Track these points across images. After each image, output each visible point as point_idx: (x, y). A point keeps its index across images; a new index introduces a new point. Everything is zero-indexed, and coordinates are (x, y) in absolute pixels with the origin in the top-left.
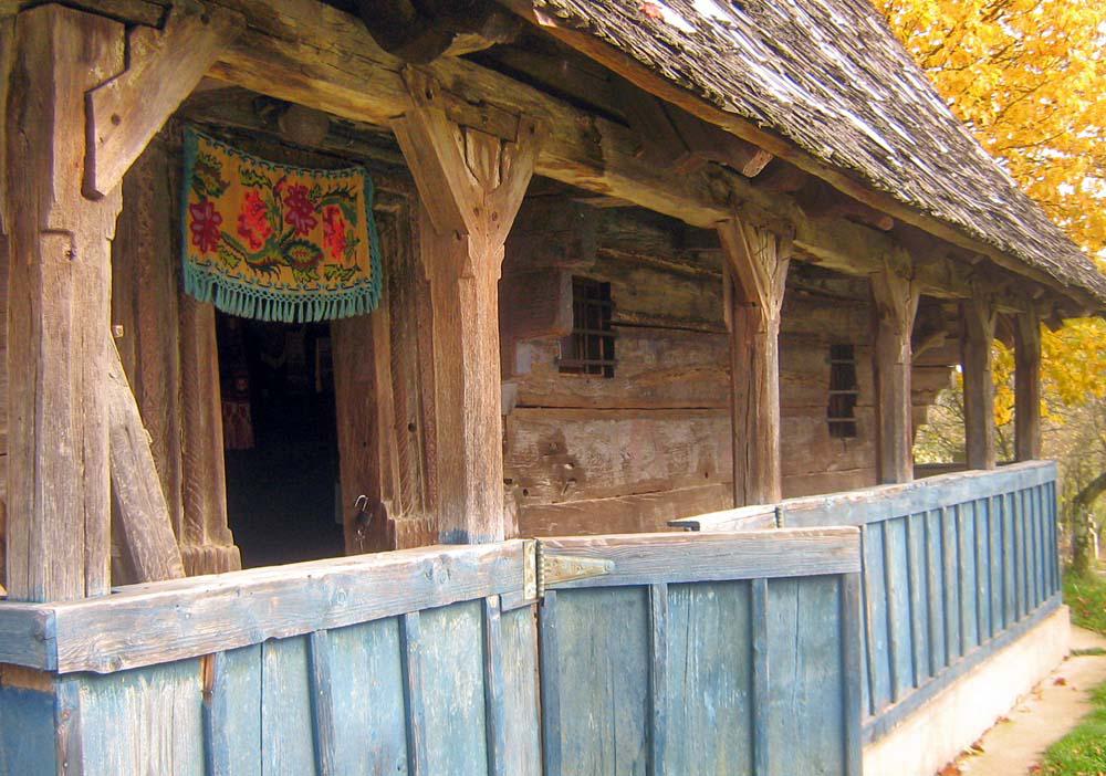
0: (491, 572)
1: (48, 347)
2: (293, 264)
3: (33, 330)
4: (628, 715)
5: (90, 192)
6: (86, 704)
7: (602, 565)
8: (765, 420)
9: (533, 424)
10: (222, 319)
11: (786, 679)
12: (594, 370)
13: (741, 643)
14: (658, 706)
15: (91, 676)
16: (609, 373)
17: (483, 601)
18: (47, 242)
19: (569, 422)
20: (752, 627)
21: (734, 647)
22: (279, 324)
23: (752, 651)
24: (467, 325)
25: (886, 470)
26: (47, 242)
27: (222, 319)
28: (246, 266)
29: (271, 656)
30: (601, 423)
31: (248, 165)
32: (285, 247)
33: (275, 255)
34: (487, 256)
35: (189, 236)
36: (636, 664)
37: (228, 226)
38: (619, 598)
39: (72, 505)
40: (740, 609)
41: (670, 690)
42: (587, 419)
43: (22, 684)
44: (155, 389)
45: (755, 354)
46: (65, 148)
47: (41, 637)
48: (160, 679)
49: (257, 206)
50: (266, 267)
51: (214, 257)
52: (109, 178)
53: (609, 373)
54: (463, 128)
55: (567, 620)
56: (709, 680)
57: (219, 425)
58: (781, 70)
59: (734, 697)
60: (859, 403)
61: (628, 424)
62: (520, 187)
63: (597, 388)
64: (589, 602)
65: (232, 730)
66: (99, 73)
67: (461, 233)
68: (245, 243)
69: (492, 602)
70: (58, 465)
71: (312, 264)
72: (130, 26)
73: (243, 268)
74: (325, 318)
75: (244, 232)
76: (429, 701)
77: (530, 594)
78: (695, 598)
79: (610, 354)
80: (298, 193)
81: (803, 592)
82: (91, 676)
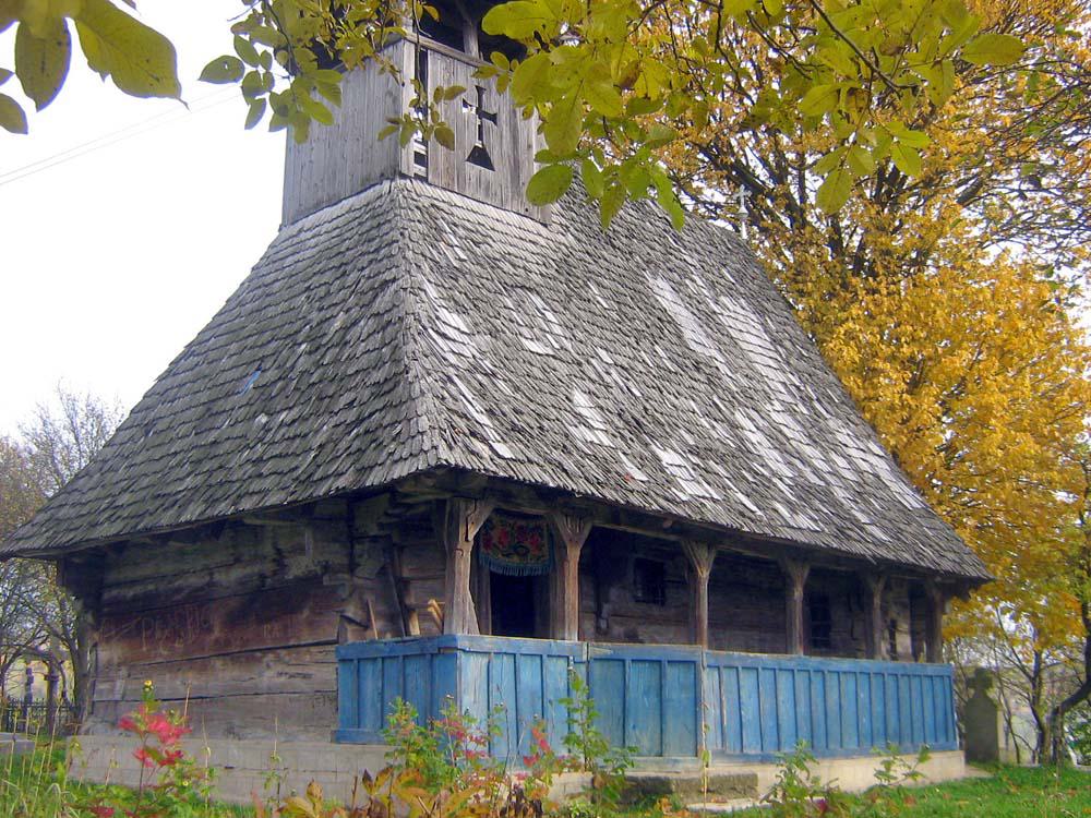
0: (571, 649)
1: (457, 577)
2: (518, 554)
3: (454, 572)
4: (618, 701)
5: (467, 540)
6: (462, 657)
7: (609, 652)
8: (700, 617)
9: (622, 624)
10: (492, 575)
11: (674, 696)
12: (655, 602)
13: (658, 681)
14: (627, 698)
15: (464, 651)
16: (663, 604)
17: (568, 658)
18: (457, 552)
19: (639, 624)
20: (661, 676)
21: (654, 682)
22: (513, 577)
23: (696, 711)
24: (567, 574)
25: (789, 649)
26: (457, 552)
27: (492, 575)
28: (940, 21)
29: (505, 657)
30: (658, 627)
31: (503, 518)
32: (515, 549)
33: (512, 551)
34: (574, 555)
35: (481, 544)
36: (620, 683)
37: (495, 541)
38: (617, 663)
39: (461, 613)
40: (658, 672)
41: (631, 695)
42: (651, 624)
43: (449, 651)
44: (476, 598)
45: (696, 591)
46: (462, 531)
47: (455, 640)
48: (479, 656)
49: (505, 534)
50: (508, 556)
51: (490, 552)
52: (471, 537)
53: (663, 604)
54: (566, 516)
55: (597, 668)
56: (646, 693)
57: (490, 612)
58: (701, 479)
59: (655, 700)
60: (833, 629)
61: (673, 628)
62: (586, 532)
63: (655, 610)
64: (606, 664)
65: (494, 672)
66: (469, 512)
67: (565, 547)
68: (501, 546)
69: (571, 658)
70: (458, 604)
71: (525, 555)
72: (476, 500)
73: (500, 556)
74: (966, 700)
75: (501, 543)
76: (549, 681)
77: (585, 658)
78: (641, 665)
79: (663, 595)
80: (521, 528)
81: (681, 666)
82: (464, 651)
